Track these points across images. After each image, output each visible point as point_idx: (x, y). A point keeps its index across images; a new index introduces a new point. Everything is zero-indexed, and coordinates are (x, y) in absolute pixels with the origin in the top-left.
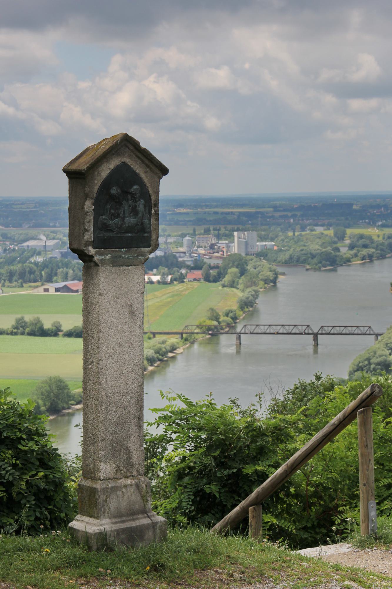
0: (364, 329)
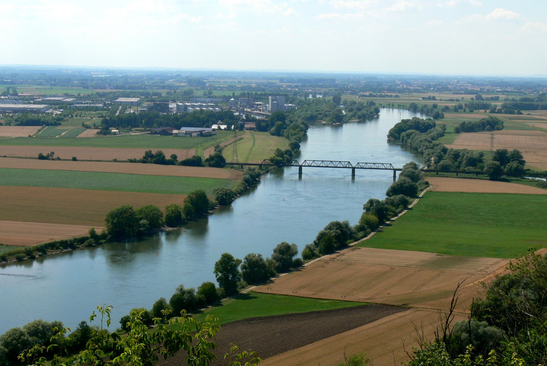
0: (327, 163)
